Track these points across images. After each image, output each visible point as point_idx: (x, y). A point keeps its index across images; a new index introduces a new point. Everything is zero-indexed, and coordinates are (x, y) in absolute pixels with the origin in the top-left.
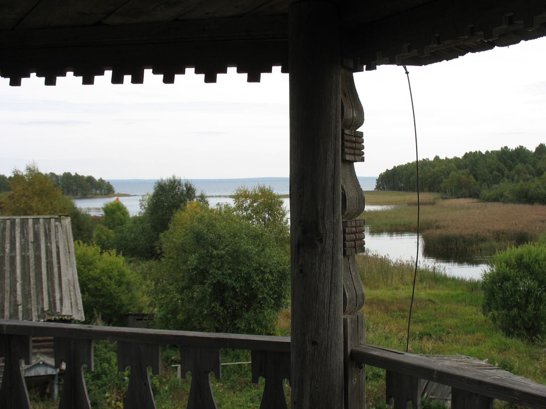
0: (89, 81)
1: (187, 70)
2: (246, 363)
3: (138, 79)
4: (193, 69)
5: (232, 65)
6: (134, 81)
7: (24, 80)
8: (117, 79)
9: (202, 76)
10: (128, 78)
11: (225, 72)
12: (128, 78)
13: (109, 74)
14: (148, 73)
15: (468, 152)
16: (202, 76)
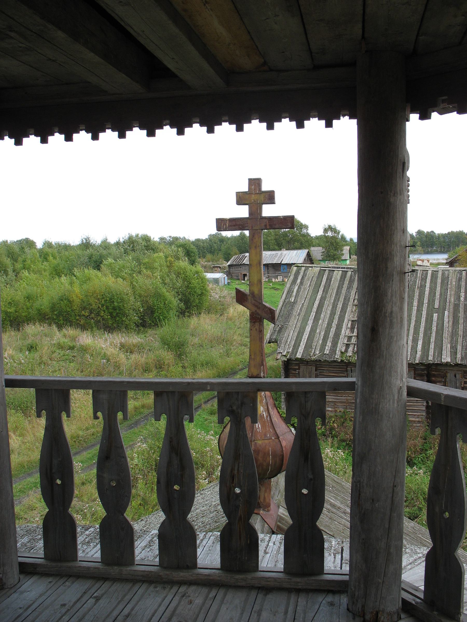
4: (418, 115)
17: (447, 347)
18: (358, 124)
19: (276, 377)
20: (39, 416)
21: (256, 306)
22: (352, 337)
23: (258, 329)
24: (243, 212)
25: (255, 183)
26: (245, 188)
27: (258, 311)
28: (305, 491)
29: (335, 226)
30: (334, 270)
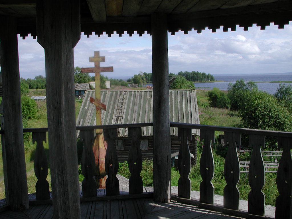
0: (214, 31)
1: (253, 25)
2: (173, 91)
3: (233, 29)
4: (273, 23)
5: (272, 21)
6: (232, 30)
7: (202, 31)
8: (225, 30)
9: (278, 26)
10: (229, 29)
11: (269, 25)
12: (229, 29)
13: (222, 28)
14: (237, 26)
15: (126, 34)
16: (278, 26)
17: (136, 120)
18: (271, 22)
19: (246, 128)
20: (33, 143)
21: (99, 104)
22: (119, 117)
23: (99, 113)
24: (92, 65)
25: (97, 53)
26: (101, 55)
27: (99, 105)
28: (135, 164)
29: (103, 75)
30: (132, 91)
